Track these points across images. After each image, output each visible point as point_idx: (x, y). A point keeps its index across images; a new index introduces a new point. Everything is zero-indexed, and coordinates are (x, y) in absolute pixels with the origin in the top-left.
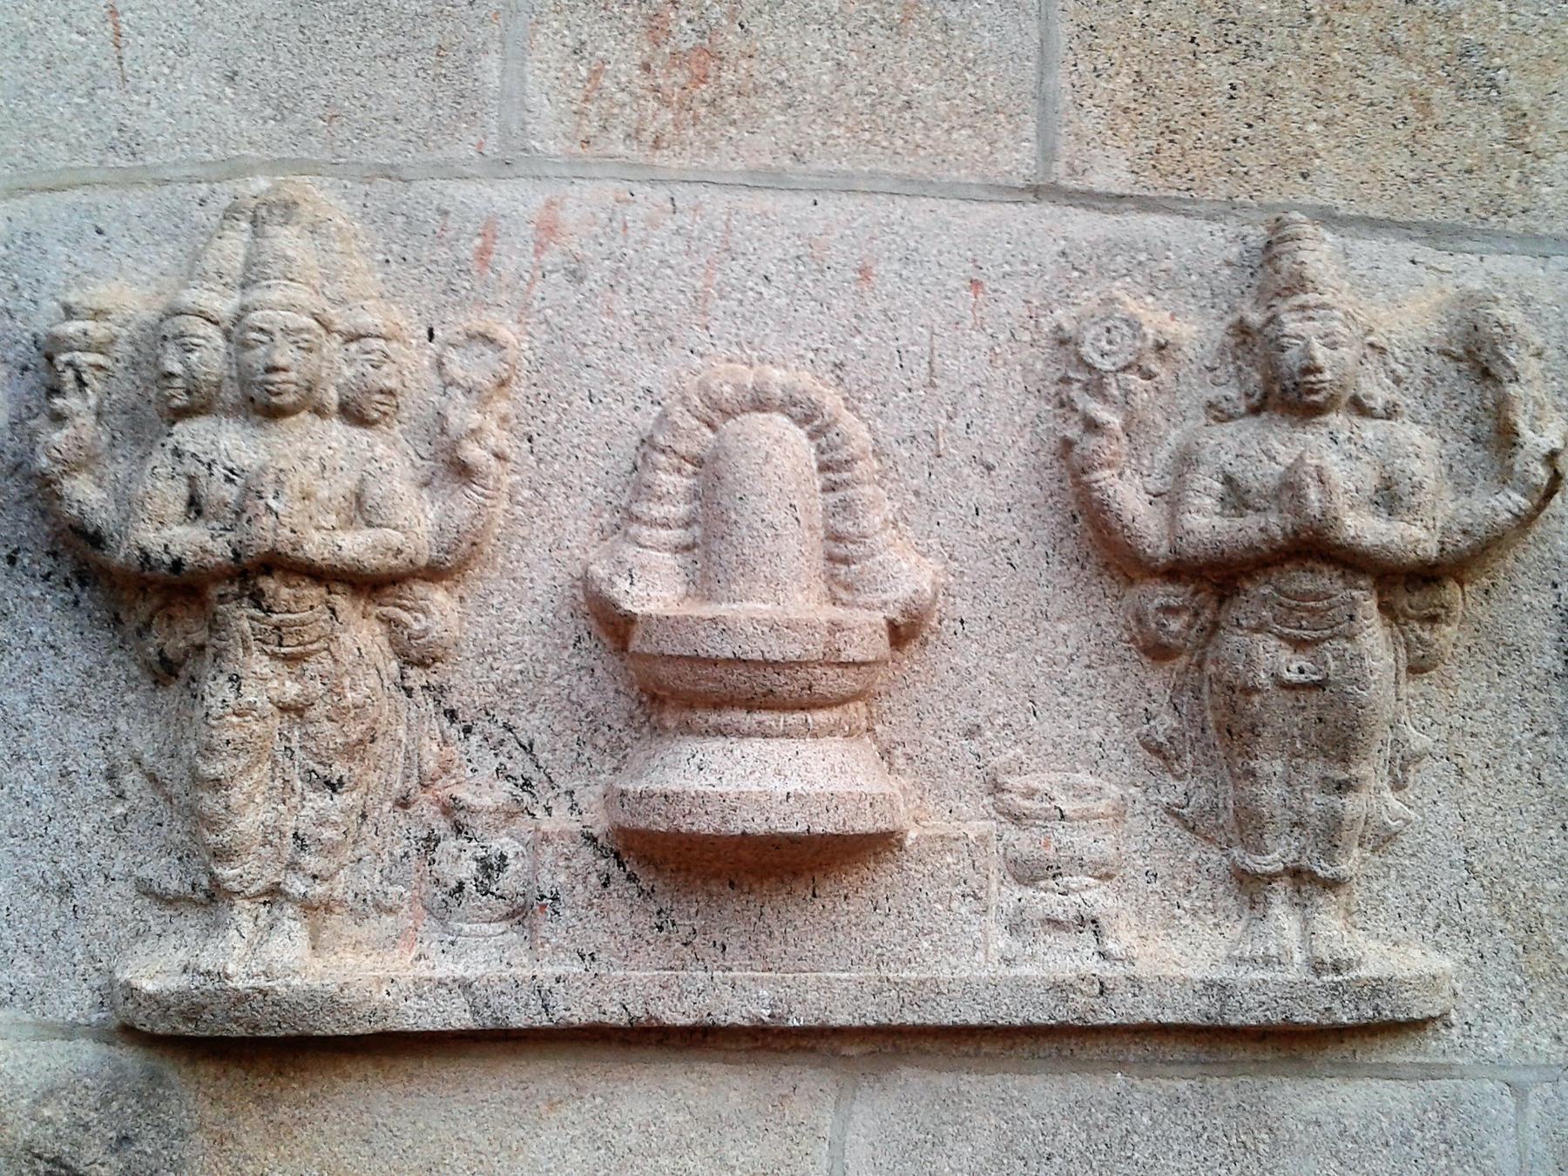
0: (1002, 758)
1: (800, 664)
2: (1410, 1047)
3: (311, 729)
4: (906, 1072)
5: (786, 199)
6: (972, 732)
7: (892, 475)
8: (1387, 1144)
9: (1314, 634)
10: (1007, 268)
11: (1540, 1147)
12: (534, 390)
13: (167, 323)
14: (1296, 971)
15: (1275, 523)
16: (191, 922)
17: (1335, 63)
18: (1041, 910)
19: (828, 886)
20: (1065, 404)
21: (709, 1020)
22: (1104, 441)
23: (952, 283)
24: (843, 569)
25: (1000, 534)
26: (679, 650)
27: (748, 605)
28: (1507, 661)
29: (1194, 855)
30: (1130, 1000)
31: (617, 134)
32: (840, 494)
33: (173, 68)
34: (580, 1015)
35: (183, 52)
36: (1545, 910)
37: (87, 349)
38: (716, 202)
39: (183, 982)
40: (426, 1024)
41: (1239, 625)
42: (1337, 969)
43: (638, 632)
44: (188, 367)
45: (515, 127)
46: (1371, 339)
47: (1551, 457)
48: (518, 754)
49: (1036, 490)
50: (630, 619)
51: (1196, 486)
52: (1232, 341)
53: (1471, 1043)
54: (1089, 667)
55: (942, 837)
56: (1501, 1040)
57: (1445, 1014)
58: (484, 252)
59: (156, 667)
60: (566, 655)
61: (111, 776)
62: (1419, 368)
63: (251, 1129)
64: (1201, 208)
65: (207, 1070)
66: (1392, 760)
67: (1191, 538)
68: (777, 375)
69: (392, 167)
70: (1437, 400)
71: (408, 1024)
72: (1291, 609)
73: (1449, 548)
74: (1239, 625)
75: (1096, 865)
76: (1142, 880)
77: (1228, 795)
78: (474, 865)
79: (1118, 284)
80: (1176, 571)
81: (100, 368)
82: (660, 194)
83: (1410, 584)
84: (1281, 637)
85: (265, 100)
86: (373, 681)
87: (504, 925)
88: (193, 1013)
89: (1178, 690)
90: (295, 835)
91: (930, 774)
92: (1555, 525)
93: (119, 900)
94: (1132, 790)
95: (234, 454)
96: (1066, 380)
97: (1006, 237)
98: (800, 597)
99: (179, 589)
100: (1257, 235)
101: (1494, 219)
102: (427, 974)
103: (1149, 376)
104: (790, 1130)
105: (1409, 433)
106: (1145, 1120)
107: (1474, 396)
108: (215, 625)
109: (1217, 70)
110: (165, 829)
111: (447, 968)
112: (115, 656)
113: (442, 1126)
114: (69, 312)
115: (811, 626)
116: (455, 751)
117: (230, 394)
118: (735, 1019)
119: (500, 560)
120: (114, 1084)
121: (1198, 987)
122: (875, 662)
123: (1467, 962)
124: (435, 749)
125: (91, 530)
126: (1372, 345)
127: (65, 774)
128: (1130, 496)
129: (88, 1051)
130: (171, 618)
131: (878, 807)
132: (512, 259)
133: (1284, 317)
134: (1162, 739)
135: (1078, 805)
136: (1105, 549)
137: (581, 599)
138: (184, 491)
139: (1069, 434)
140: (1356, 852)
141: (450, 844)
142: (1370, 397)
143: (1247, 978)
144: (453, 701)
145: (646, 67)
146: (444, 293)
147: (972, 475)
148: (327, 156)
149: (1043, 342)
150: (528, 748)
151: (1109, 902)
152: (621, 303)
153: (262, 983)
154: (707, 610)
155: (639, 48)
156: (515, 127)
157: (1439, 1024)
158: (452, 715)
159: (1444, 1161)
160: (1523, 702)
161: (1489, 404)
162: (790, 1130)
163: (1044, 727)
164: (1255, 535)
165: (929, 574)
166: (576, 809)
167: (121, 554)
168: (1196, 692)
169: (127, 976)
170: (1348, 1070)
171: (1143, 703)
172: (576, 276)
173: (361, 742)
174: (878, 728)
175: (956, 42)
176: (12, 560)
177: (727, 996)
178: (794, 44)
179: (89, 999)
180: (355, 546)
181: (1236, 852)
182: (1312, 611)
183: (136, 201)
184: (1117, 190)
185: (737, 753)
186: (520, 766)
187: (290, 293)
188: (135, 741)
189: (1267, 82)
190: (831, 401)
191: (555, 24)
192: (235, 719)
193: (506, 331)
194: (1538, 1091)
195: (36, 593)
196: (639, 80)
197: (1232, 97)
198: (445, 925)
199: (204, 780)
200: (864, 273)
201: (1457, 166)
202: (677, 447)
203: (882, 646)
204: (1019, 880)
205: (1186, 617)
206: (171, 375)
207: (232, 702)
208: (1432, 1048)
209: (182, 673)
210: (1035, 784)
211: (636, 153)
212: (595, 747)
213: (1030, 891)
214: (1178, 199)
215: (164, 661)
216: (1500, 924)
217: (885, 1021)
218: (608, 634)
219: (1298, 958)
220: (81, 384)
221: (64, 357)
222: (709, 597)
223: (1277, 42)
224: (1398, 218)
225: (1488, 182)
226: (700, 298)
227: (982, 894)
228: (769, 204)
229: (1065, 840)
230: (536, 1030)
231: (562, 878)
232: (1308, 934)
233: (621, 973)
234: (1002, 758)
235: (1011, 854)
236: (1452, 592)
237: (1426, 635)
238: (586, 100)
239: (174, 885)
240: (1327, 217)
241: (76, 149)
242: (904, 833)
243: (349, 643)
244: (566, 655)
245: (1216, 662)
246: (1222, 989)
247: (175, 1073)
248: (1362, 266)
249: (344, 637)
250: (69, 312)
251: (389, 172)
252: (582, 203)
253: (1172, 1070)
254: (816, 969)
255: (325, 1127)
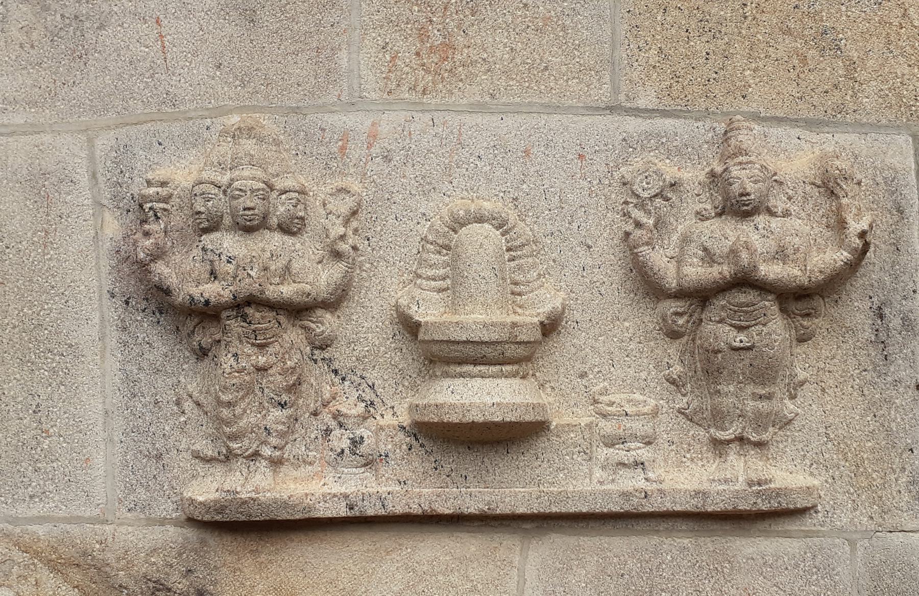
0: (598, 388)
1: (498, 343)
2: (798, 523)
3: (271, 379)
4: (554, 536)
5: (487, 117)
6: (583, 375)
7: (542, 252)
8: (787, 568)
9: (747, 323)
10: (597, 148)
11: (863, 570)
12: (369, 215)
13: (197, 187)
14: (740, 485)
15: (725, 270)
16: (218, 469)
17: (758, 40)
18: (617, 459)
19: (515, 448)
20: (627, 215)
21: (459, 511)
22: (644, 232)
23: (570, 157)
24: (519, 298)
25: (595, 279)
26: (442, 338)
27: (472, 316)
28: (847, 335)
29: (692, 433)
30: (660, 500)
31: (405, 88)
32: (516, 262)
33: (191, 63)
34: (399, 509)
35: (195, 54)
36: (865, 456)
37: (159, 201)
38: (454, 120)
39: (217, 495)
40: (329, 514)
41: (711, 320)
42: (759, 484)
43: (422, 330)
44: (208, 209)
45: (356, 87)
46: (774, 178)
47: (862, 235)
48: (367, 390)
49: (613, 257)
50: (418, 325)
51: (689, 253)
52: (708, 181)
53: (828, 520)
54: (640, 343)
55: (568, 425)
56: (843, 519)
57: (814, 507)
58: (343, 148)
59: (198, 352)
60: (388, 342)
61: (178, 403)
62: (800, 192)
63: (248, 564)
64: (693, 115)
65: (227, 539)
66: (789, 384)
67: (687, 278)
68: (487, 205)
69: (298, 108)
70: (809, 207)
71: (320, 514)
72: (735, 311)
73: (813, 279)
74: (711, 320)
75: (643, 437)
76: (666, 445)
77: (708, 403)
78: (349, 441)
79: (652, 154)
80: (681, 294)
81: (165, 210)
82: (427, 117)
83: (797, 299)
84: (731, 325)
85: (236, 77)
86: (299, 356)
87: (363, 469)
88: (221, 509)
89: (683, 353)
90: (266, 428)
91: (563, 396)
92: (871, 267)
93: (185, 461)
94: (661, 402)
95: (230, 250)
96: (626, 203)
97: (596, 133)
98: (498, 312)
99: (207, 314)
100: (721, 128)
101: (839, 116)
102: (329, 491)
103: (667, 199)
104: (499, 563)
105: (794, 223)
106: (669, 557)
107: (826, 205)
108: (225, 332)
109: (699, 45)
110: (204, 427)
111: (337, 489)
112: (178, 347)
113: (336, 562)
114: (149, 183)
115: (503, 325)
116: (338, 388)
117: (227, 220)
118: (472, 510)
119: (356, 298)
120: (183, 546)
121: (693, 493)
122: (534, 342)
123: (826, 481)
124: (329, 388)
125: (165, 288)
126: (775, 181)
127: (157, 403)
128: (660, 259)
129: (172, 531)
130: (204, 328)
131: (536, 409)
132: (356, 152)
133: (732, 169)
134: (675, 377)
135: (634, 409)
136: (649, 286)
137: (395, 316)
138: (208, 267)
139: (627, 229)
140: (771, 429)
141: (337, 432)
142: (776, 207)
143: (716, 489)
144: (336, 365)
145: (418, 54)
146: (325, 169)
147: (581, 250)
148: (266, 104)
149: (615, 184)
150: (372, 387)
151: (650, 455)
152: (409, 171)
153: (253, 495)
154: (456, 318)
155: (414, 45)
156: (356, 87)
157: (812, 512)
158: (336, 372)
159: (815, 577)
160: (855, 355)
161: (834, 208)
162: (499, 563)
163: (617, 372)
164: (716, 274)
165: (561, 300)
166: (397, 413)
167: (180, 298)
168: (692, 354)
169: (190, 495)
170: (767, 534)
171: (666, 360)
172: (387, 159)
173: (294, 385)
174: (538, 374)
175: (569, 36)
176: (127, 303)
177: (467, 500)
178: (490, 40)
179: (172, 507)
180: (288, 291)
181: (712, 430)
182: (746, 312)
183: (176, 128)
184: (650, 107)
185: (470, 385)
186: (369, 395)
187: (253, 172)
188: (189, 386)
189: (725, 51)
190: (513, 217)
191: (374, 35)
192: (237, 374)
193: (356, 187)
194: (862, 543)
195: (139, 318)
196: (415, 62)
197: (707, 59)
198: (336, 470)
199: (222, 403)
200: (527, 152)
201: (820, 89)
202: (438, 241)
203: (538, 335)
204: (606, 445)
205: (686, 318)
206: (199, 213)
207: (235, 366)
208: (808, 523)
209: (210, 354)
210: (613, 400)
211: (414, 97)
212: (403, 386)
213: (612, 450)
214: (681, 110)
215: (201, 348)
216: (843, 463)
217: (542, 510)
218: (409, 333)
219: (741, 479)
220: (158, 218)
221: (149, 205)
222: (456, 312)
223: (730, 30)
224: (791, 116)
225: (836, 97)
226: (448, 168)
227: (588, 451)
228: (480, 120)
229: (628, 425)
230: (379, 517)
231: (390, 447)
232: (747, 468)
233: (418, 490)
234: (598, 388)
235: (602, 433)
236: (818, 302)
237: (805, 323)
238: (390, 71)
239: (210, 453)
240: (756, 117)
241: (146, 104)
242: (550, 423)
243: (287, 338)
244: (388, 342)
245: (700, 338)
246: (705, 494)
247: (213, 540)
248: (772, 141)
249: (285, 336)
250: (149, 183)
251: (296, 110)
252: (389, 123)
253: (681, 534)
254: (512, 487)
255: (283, 564)
